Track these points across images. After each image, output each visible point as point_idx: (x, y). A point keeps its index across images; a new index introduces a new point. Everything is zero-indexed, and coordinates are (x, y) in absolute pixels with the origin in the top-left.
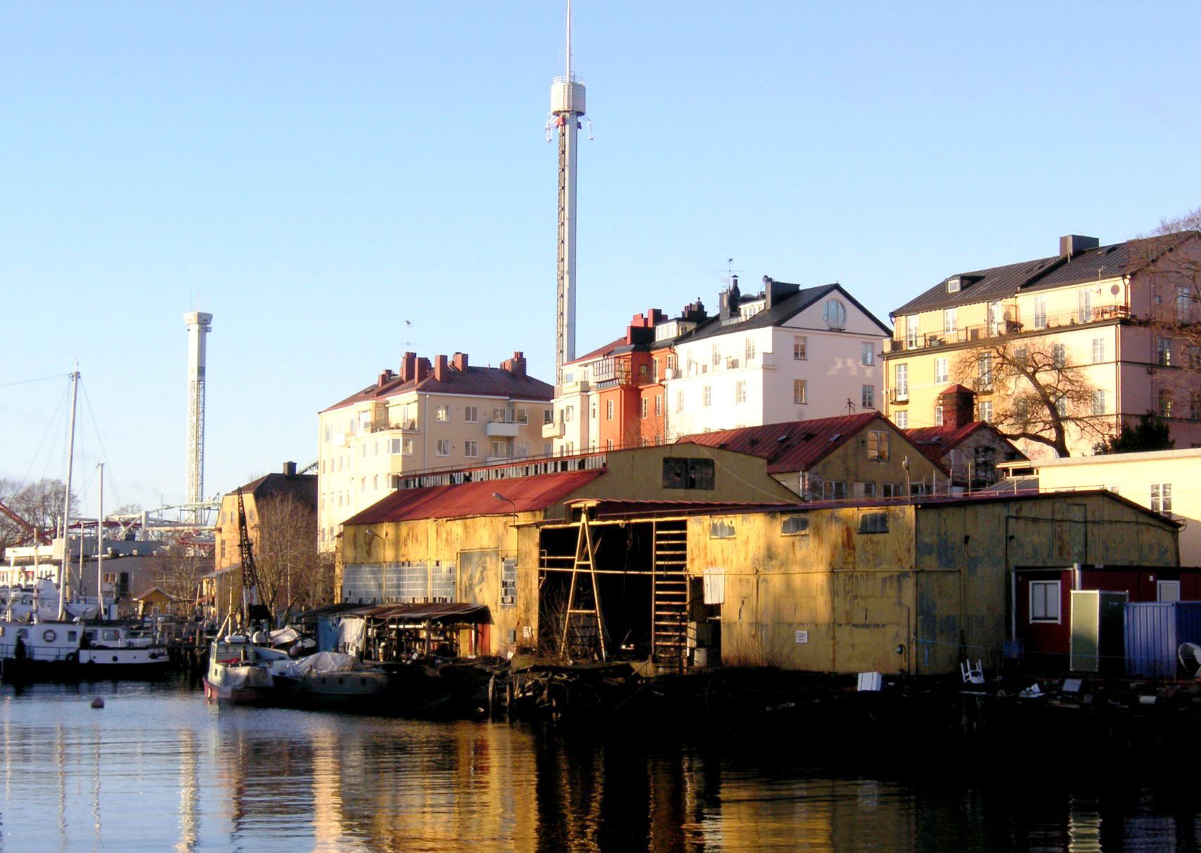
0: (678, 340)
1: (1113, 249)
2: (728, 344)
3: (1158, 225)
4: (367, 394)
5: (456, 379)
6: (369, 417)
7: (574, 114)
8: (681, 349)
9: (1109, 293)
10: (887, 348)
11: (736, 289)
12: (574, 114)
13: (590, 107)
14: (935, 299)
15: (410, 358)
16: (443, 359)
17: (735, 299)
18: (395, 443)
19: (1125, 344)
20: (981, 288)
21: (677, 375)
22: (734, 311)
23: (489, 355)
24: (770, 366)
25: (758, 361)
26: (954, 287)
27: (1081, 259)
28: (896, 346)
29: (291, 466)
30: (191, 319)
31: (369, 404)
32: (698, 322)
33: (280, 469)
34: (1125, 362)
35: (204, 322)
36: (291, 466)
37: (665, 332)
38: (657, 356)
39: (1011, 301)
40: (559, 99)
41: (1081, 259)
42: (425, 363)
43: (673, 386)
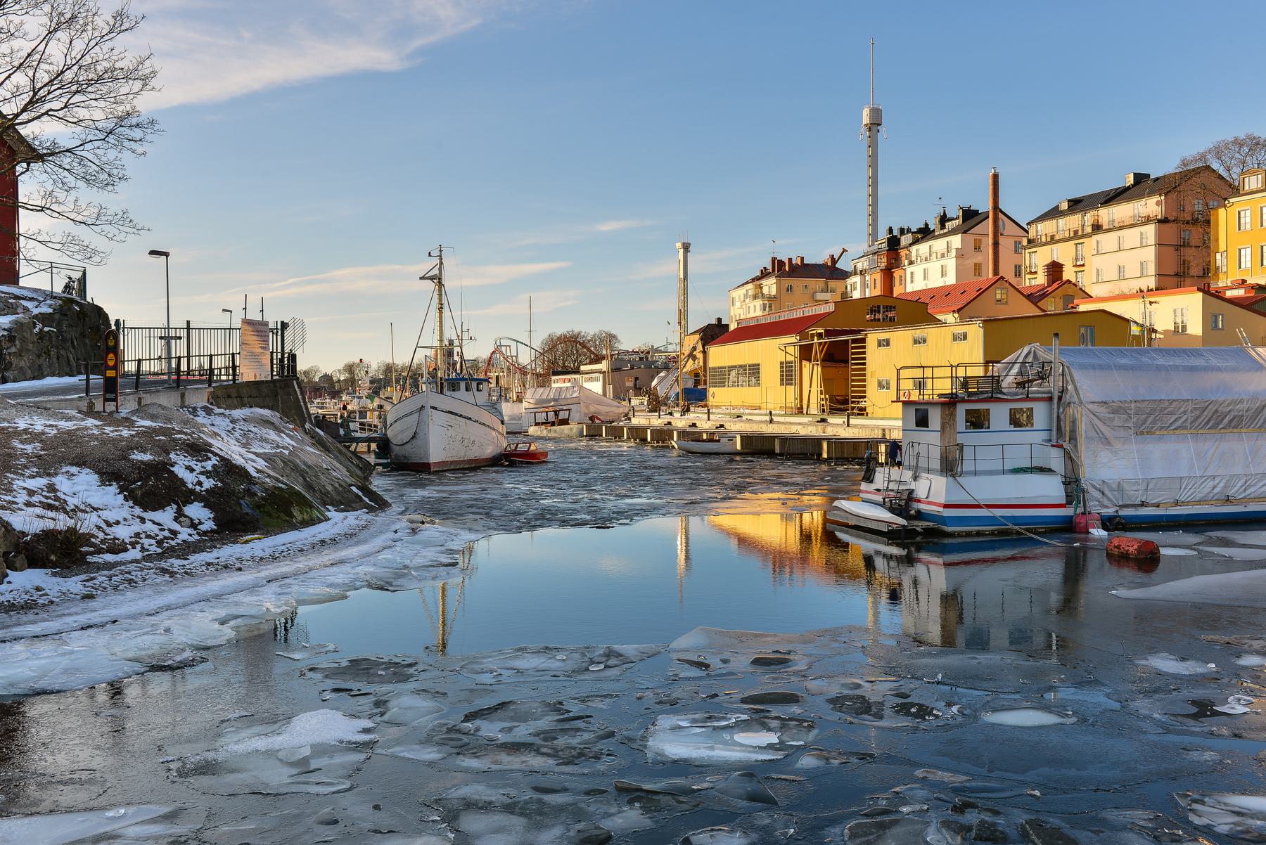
0: (911, 245)
1: (1158, 179)
2: (939, 245)
3: (1178, 162)
4: (753, 280)
5: (802, 270)
6: (751, 293)
7: (875, 125)
8: (914, 249)
9: (1151, 206)
10: (1025, 243)
11: (945, 214)
12: (875, 125)
13: (885, 119)
14: (1054, 213)
15: (774, 260)
16: (790, 260)
17: (944, 220)
18: (764, 305)
19: (1159, 235)
20: (1081, 205)
21: (911, 263)
22: (943, 227)
23: (818, 256)
24: (960, 255)
25: (953, 253)
26: (1065, 206)
27: (1142, 184)
28: (1030, 241)
29: (719, 320)
30: (679, 245)
31: (750, 286)
32: (925, 233)
33: (714, 322)
34: (1160, 244)
35: (686, 247)
36: (719, 320)
37: (906, 240)
38: (903, 253)
39: (1094, 212)
40: (866, 119)
41: (1142, 184)
42: (781, 263)
43: (909, 269)
